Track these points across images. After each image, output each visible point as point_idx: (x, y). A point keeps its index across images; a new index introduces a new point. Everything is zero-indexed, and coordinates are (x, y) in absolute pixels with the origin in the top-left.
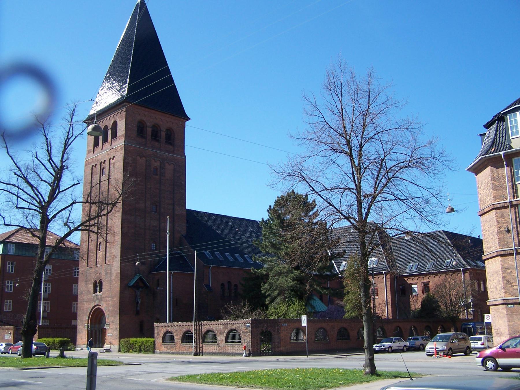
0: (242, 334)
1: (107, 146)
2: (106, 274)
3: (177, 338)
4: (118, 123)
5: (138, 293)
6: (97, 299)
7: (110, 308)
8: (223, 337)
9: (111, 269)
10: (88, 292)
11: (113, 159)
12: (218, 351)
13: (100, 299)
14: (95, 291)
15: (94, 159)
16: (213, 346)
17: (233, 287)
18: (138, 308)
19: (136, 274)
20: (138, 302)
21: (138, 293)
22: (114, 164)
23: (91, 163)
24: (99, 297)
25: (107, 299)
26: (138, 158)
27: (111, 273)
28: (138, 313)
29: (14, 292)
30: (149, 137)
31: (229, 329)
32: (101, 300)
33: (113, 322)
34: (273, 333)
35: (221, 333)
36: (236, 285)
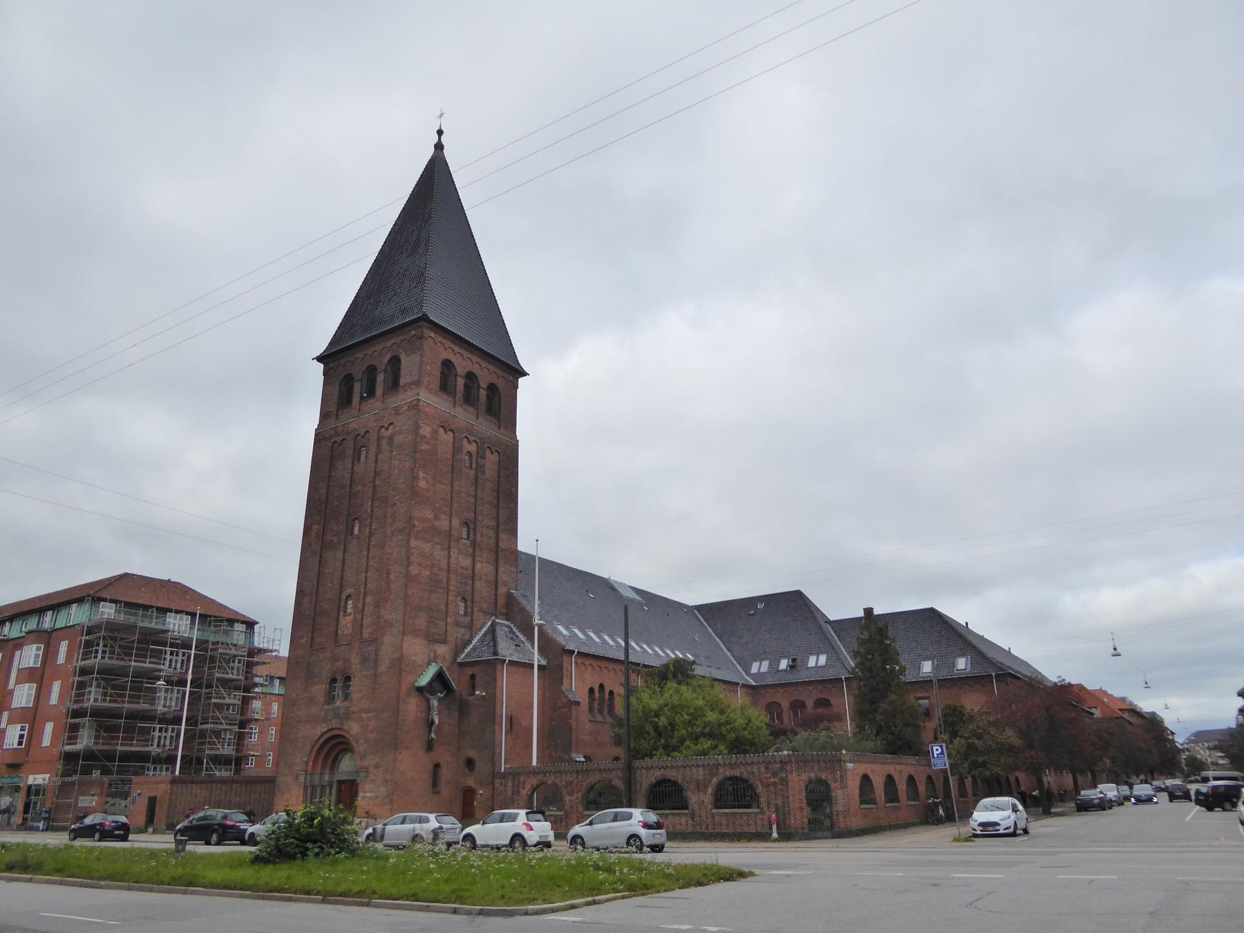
0: (760, 789)
1: (375, 405)
2: (364, 660)
3: (701, 800)
4: (403, 362)
5: (435, 703)
6: (337, 716)
7: (371, 736)
8: (707, 797)
9: (377, 651)
10: (312, 701)
11: (387, 429)
12: (690, 829)
13: (347, 716)
14: (330, 699)
15: (340, 429)
16: (677, 818)
17: (607, 696)
18: (433, 735)
19: (429, 664)
20: (433, 722)
21: (435, 703)
22: (391, 438)
23: (331, 436)
24: (342, 711)
25: (364, 715)
26: (441, 430)
27: (376, 660)
28: (430, 746)
29: (134, 702)
30: (460, 395)
31: (720, 777)
32: (347, 718)
33: (377, 766)
34: (833, 785)
35: (700, 787)
36: (611, 693)
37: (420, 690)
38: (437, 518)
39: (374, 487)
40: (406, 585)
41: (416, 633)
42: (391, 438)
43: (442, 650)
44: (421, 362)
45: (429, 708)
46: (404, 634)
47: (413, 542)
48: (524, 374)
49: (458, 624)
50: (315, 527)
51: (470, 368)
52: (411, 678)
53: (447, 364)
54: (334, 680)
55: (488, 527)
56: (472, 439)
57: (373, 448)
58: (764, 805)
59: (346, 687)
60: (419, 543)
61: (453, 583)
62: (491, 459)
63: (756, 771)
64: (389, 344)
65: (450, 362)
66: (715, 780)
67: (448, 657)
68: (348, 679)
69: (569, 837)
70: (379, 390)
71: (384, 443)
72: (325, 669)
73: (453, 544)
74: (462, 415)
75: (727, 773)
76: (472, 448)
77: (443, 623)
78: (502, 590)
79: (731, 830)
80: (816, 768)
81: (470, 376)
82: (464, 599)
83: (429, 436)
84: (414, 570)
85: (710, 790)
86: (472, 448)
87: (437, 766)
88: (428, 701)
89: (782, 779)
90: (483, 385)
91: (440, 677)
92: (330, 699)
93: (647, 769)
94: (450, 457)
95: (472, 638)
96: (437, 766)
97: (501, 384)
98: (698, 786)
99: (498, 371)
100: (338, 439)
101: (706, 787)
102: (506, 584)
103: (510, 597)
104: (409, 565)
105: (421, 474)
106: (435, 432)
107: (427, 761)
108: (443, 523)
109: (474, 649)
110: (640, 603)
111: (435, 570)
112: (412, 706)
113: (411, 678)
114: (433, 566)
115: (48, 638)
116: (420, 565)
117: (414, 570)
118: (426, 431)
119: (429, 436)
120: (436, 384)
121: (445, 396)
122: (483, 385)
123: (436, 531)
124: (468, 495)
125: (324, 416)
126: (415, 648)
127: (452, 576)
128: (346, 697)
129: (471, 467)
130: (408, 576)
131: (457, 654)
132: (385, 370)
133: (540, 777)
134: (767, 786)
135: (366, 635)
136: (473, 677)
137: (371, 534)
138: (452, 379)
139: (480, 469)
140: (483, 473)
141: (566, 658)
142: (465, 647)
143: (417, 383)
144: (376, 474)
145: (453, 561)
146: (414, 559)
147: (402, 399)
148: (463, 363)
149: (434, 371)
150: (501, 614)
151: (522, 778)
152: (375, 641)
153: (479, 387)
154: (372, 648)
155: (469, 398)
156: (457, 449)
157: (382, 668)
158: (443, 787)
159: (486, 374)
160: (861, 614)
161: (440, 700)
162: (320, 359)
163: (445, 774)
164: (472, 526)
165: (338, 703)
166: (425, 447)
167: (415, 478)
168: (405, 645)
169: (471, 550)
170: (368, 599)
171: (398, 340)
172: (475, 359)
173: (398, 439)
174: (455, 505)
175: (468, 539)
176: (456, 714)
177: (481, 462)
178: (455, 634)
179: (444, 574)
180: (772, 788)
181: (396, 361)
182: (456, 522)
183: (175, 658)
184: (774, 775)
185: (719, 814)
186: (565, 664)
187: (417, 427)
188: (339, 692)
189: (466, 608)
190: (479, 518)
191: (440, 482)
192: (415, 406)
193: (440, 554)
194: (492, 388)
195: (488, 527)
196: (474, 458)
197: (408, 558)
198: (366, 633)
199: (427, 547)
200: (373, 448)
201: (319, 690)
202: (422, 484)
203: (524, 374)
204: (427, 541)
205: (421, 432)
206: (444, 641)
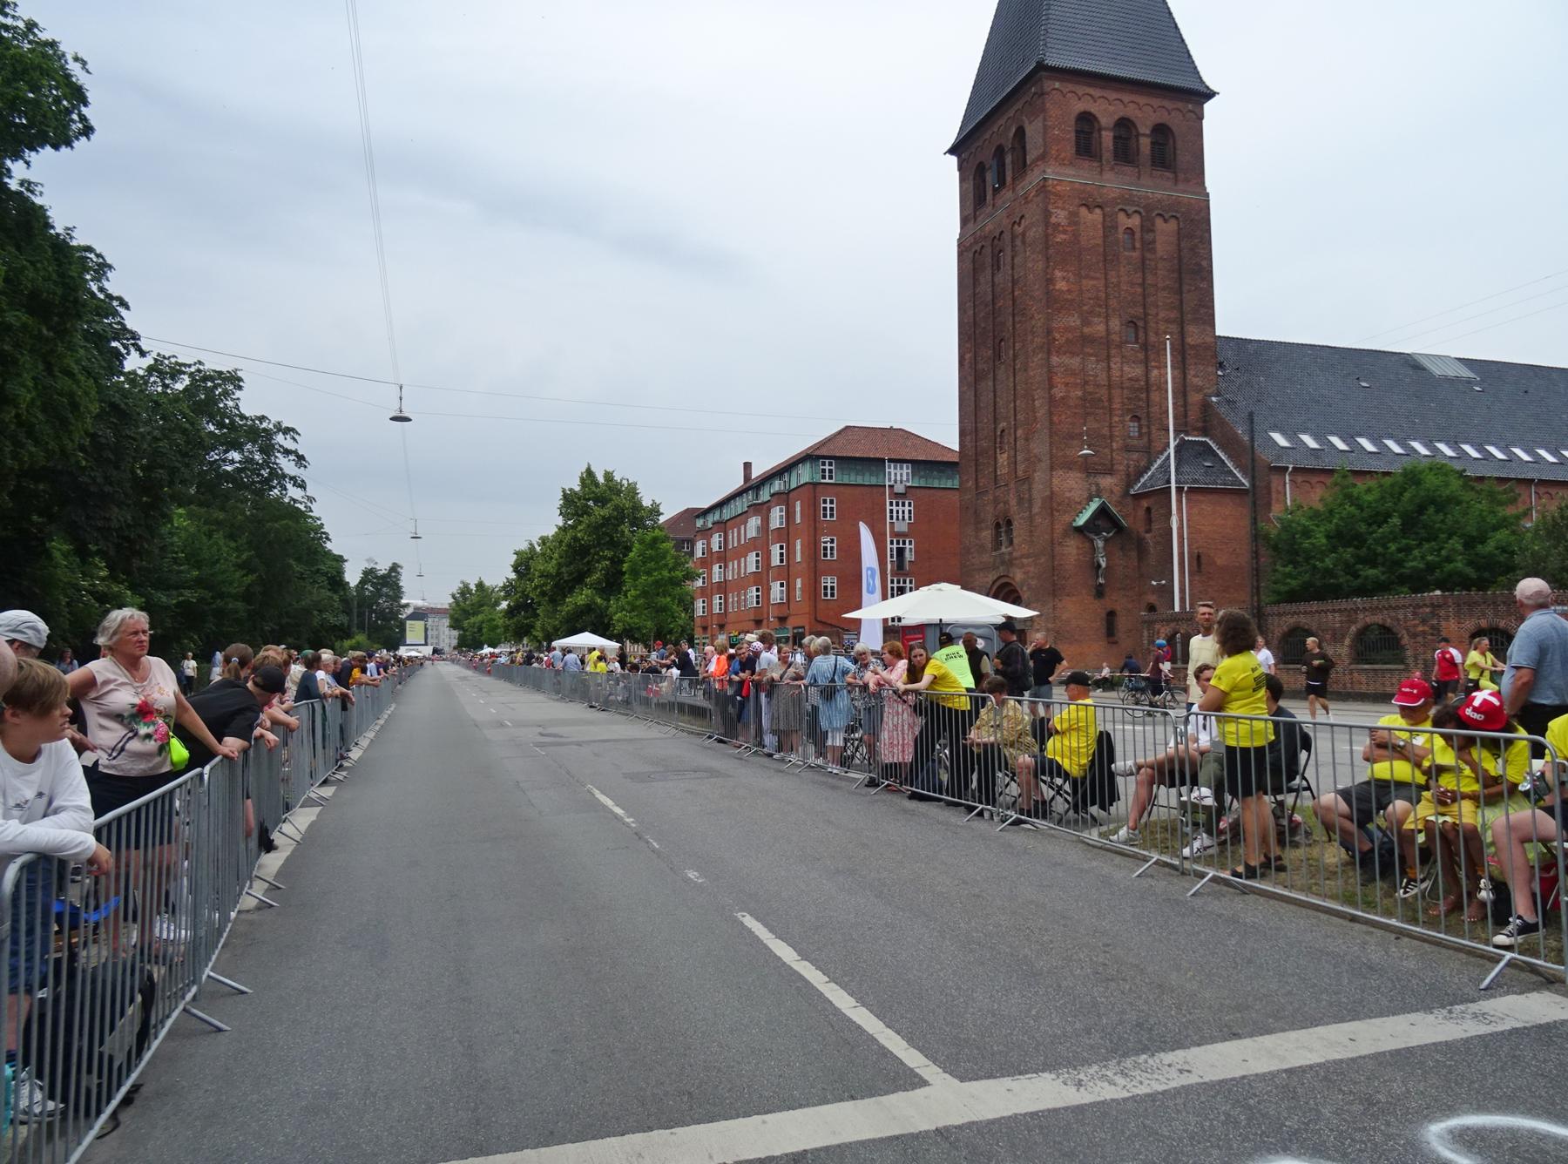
0: (1406, 640)
1: (1007, 194)
2: (1020, 501)
6: (1003, 563)
7: (1033, 583)
9: (1030, 490)
10: (982, 548)
13: (1010, 563)
14: (997, 545)
18: (1101, 580)
19: (1090, 499)
20: (1099, 566)
21: (1100, 544)
22: (1023, 234)
26: (1083, 210)
27: (1030, 501)
28: (1100, 592)
30: (1107, 155)
31: (1360, 625)
37: (1079, 530)
38: (1086, 323)
39: (1014, 300)
40: (1051, 413)
41: (1069, 465)
42: (1023, 234)
43: (1107, 482)
44: (1045, 126)
45: (1093, 549)
46: (1052, 469)
47: (1055, 360)
48: (1210, 95)
49: (1128, 449)
50: (968, 356)
51: (1121, 112)
52: (1067, 518)
53: (1086, 119)
54: (998, 525)
55: (1168, 321)
56: (1131, 209)
57: (1008, 250)
58: (1410, 661)
59: (1009, 531)
60: (1066, 360)
61: (1117, 400)
62: (1165, 231)
63: (1401, 617)
64: (1011, 113)
65: (1090, 114)
66: (1353, 628)
67: (1117, 489)
68: (1009, 523)
69: (339, 690)
70: (1009, 179)
71: (1018, 242)
72: (989, 515)
73: (1113, 352)
74: (1113, 182)
75: (1368, 620)
76: (1135, 221)
77: (1107, 451)
78: (1195, 398)
79: (1371, 690)
80: (1490, 613)
81: (1124, 126)
82: (1136, 418)
83: (1064, 222)
84: (1059, 392)
85: (1347, 642)
86: (1135, 221)
87: (1111, 614)
88: (1092, 541)
89: (1432, 627)
90: (1144, 129)
91: (1103, 512)
92: (997, 545)
93: (1279, 615)
94: (1100, 241)
95: (1150, 464)
96: (1111, 614)
97: (1175, 121)
98: (1334, 635)
99: (1167, 103)
100: (977, 247)
101: (1343, 637)
102: (1199, 389)
103: (1206, 406)
104: (1051, 386)
105: (1058, 274)
106: (1073, 215)
107: (1099, 608)
108: (1098, 328)
109: (1151, 478)
110: (1469, 382)
111: (1090, 389)
112: (1072, 549)
113: (1067, 518)
114: (1086, 383)
115: (784, 498)
116: (1067, 384)
117: (1059, 392)
118: (1060, 216)
119: (1064, 222)
120: (1070, 150)
121: (1086, 164)
122: (1144, 129)
123: (1087, 340)
124: (1132, 284)
125: (964, 221)
126: (1071, 483)
127: (1116, 392)
128: (1011, 543)
129: (1134, 248)
130: (1052, 400)
131: (1129, 485)
132: (1013, 148)
133: (1173, 625)
134: (1414, 636)
135: (1020, 473)
136: (1148, 510)
137: (1015, 357)
138: (1095, 135)
139: (1148, 246)
140: (1153, 251)
141: (1275, 480)
142: (1141, 475)
143: (1043, 157)
144: (1014, 282)
145: (1116, 373)
146: (1057, 379)
147: (1033, 179)
148: (1107, 109)
149: (1066, 133)
150: (1195, 429)
151: (1157, 626)
152: (1028, 479)
153: (1138, 135)
154: (1026, 487)
155: (1125, 153)
156: (1109, 227)
157: (1036, 510)
158: (1121, 634)
159: (1146, 112)
160: (646, 503)
161: (1106, 540)
162: (952, 151)
163: (1122, 623)
164: (1141, 324)
165: (1003, 549)
166: (1060, 238)
167: (1050, 281)
168: (1055, 481)
169: (1141, 356)
170: (1019, 432)
171: (1019, 105)
172: (1126, 98)
173: (1031, 234)
174: (1113, 303)
175: (1137, 342)
176: (1134, 554)
177: (1149, 237)
178: (1123, 462)
179: (1103, 392)
180: (1420, 639)
181: (1021, 132)
182: (1115, 324)
183: (900, 508)
184: (1424, 622)
185: (1359, 671)
186: (1274, 486)
187: (1047, 214)
188: (1003, 538)
189: (1140, 427)
190: (1152, 311)
191: (1087, 277)
192: (1043, 188)
193: (1094, 367)
194: (1161, 130)
195: (1168, 321)
196: (1138, 236)
197: (1050, 379)
198: (1021, 468)
199: (1075, 362)
200: (1008, 250)
201: (987, 534)
202: (1061, 285)
203: (1210, 95)
204: (1073, 354)
205: (1053, 220)
206: (1110, 471)
